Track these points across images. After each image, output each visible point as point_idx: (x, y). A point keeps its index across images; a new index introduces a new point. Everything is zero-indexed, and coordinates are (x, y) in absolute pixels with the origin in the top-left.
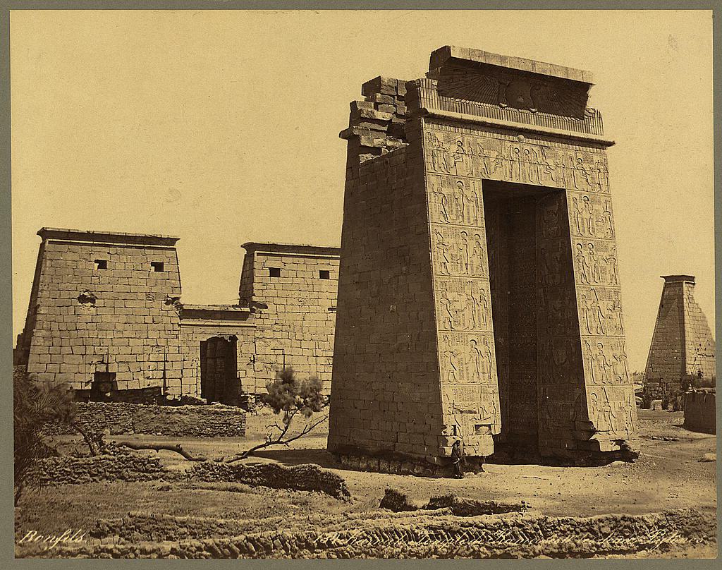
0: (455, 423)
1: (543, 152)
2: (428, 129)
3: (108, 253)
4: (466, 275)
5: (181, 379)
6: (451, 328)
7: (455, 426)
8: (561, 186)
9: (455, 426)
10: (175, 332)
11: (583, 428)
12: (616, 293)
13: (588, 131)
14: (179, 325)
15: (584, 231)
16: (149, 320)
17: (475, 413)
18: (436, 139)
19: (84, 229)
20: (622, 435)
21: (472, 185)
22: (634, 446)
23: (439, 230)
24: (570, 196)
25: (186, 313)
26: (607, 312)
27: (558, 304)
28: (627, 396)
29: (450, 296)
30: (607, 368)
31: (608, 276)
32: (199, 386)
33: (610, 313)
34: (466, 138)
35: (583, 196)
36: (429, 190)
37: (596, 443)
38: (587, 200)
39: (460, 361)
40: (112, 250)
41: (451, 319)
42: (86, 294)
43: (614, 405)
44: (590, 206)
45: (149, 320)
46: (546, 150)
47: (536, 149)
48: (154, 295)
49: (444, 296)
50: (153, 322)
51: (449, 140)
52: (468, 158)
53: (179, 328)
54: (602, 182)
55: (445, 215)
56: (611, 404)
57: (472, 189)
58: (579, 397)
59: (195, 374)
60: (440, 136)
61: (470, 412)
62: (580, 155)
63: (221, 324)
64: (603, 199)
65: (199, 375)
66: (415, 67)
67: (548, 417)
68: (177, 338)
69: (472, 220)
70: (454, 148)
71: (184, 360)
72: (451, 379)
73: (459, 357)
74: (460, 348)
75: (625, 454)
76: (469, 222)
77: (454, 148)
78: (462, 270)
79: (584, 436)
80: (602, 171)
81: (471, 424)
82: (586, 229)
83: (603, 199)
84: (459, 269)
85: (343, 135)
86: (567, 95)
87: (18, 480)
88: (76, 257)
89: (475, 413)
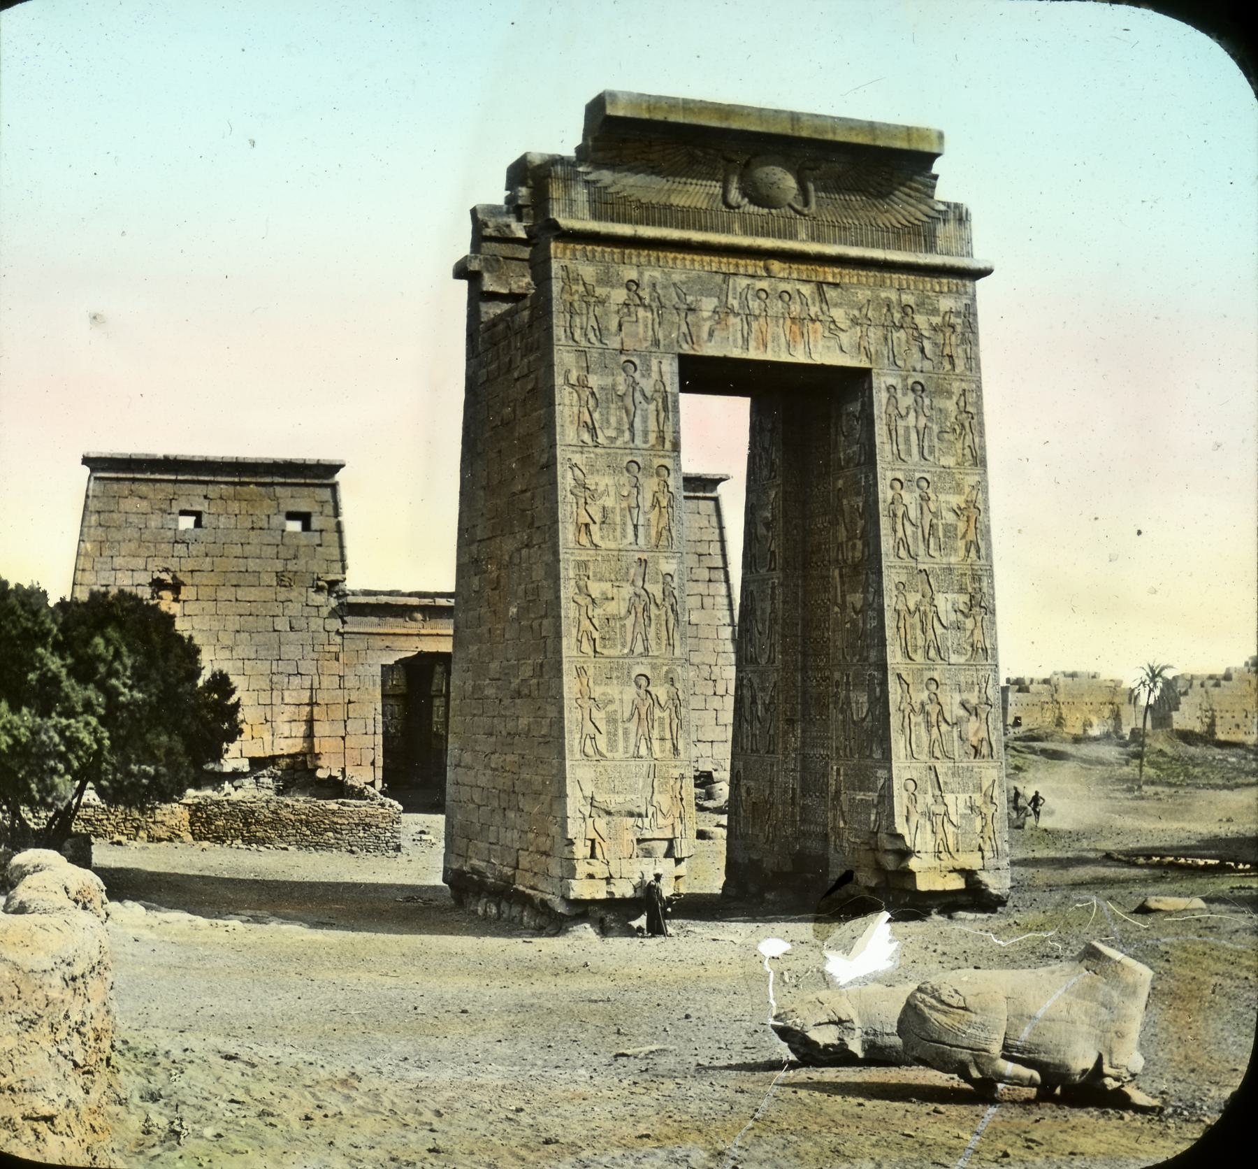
0: (593, 835)
1: (823, 299)
2: (560, 257)
3: (205, 497)
4: (635, 547)
5: (343, 738)
6: (595, 651)
7: (593, 841)
8: (865, 364)
9: (593, 841)
10: (333, 649)
11: (889, 847)
12: (976, 578)
13: (931, 248)
14: (341, 634)
15: (909, 453)
16: (282, 624)
17: (640, 815)
18: (578, 279)
19: (159, 451)
20: (972, 861)
21: (655, 368)
22: (996, 883)
23: (577, 458)
24: (882, 381)
25: (350, 609)
26: (953, 617)
27: (857, 599)
28: (986, 784)
29: (596, 589)
30: (944, 727)
31: (961, 544)
32: (380, 751)
33: (960, 617)
34: (647, 275)
35: (910, 381)
36: (559, 380)
37: (911, 874)
38: (918, 389)
39: (611, 720)
40: (213, 491)
41: (596, 635)
42: (164, 576)
43: (956, 803)
44: (927, 401)
45: (282, 624)
46: (831, 294)
47: (806, 290)
48: (290, 575)
49: (582, 590)
50: (291, 628)
51: (605, 280)
52: (649, 314)
53: (338, 639)
54: (959, 353)
55: (593, 431)
56: (949, 798)
57: (655, 376)
58: (883, 787)
59: (371, 729)
60: (588, 272)
61: (631, 814)
62: (908, 299)
63: (423, 632)
64: (956, 387)
65: (380, 730)
66: (563, 136)
67: (842, 824)
68: (337, 659)
69: (652, 438)
70: (620, 295)
71: (350, 702)
72: (589, 750)
73: (610, 708)
74: (613, 690)
75: (974, 897)
76: (646, 442)
77: (620, 295)
78: (624, 536)
79: (890, 862)
80: (959, 329)
81: (631, 836)
82: (915, 450)
83: (956, 387)
84: (618, 534)
85: (461, 271)
86: (882, 169)
87: (553, 922)
88: (143, 506)
89: (640, 815)
